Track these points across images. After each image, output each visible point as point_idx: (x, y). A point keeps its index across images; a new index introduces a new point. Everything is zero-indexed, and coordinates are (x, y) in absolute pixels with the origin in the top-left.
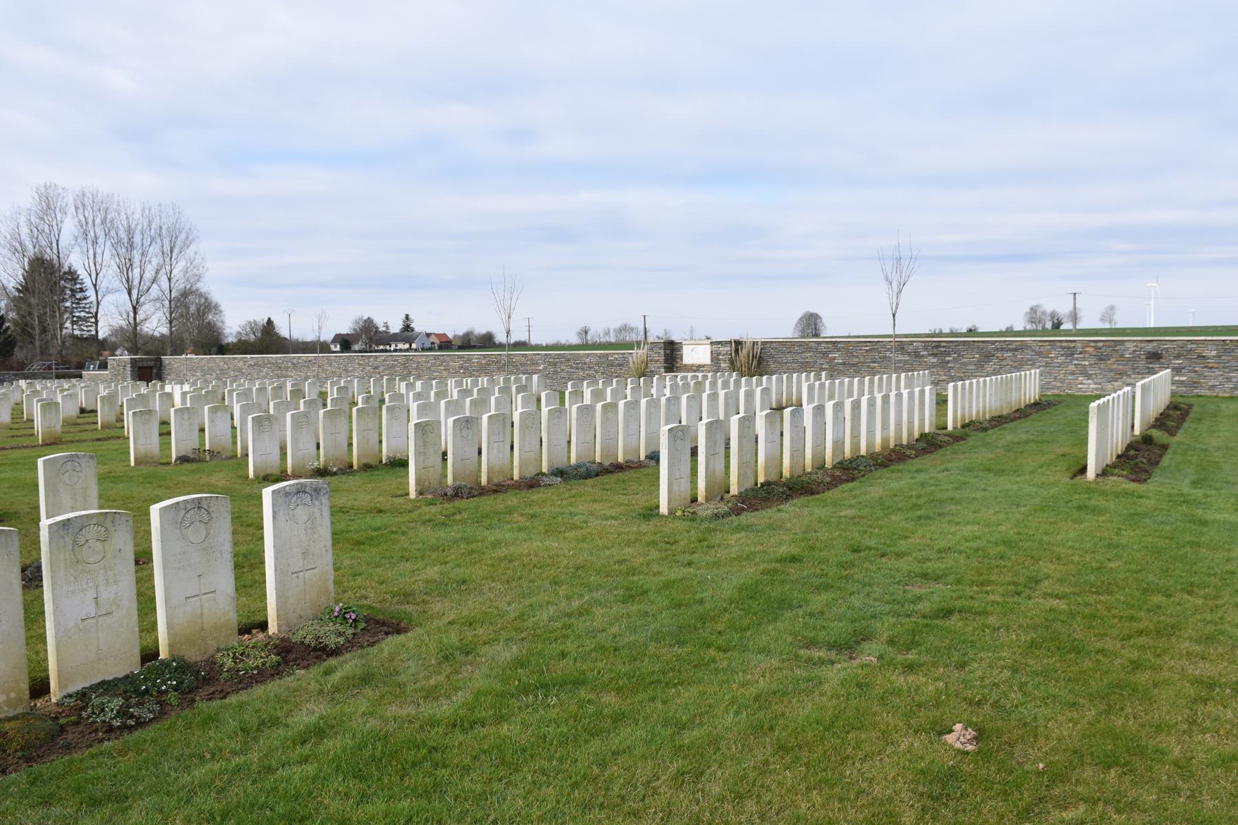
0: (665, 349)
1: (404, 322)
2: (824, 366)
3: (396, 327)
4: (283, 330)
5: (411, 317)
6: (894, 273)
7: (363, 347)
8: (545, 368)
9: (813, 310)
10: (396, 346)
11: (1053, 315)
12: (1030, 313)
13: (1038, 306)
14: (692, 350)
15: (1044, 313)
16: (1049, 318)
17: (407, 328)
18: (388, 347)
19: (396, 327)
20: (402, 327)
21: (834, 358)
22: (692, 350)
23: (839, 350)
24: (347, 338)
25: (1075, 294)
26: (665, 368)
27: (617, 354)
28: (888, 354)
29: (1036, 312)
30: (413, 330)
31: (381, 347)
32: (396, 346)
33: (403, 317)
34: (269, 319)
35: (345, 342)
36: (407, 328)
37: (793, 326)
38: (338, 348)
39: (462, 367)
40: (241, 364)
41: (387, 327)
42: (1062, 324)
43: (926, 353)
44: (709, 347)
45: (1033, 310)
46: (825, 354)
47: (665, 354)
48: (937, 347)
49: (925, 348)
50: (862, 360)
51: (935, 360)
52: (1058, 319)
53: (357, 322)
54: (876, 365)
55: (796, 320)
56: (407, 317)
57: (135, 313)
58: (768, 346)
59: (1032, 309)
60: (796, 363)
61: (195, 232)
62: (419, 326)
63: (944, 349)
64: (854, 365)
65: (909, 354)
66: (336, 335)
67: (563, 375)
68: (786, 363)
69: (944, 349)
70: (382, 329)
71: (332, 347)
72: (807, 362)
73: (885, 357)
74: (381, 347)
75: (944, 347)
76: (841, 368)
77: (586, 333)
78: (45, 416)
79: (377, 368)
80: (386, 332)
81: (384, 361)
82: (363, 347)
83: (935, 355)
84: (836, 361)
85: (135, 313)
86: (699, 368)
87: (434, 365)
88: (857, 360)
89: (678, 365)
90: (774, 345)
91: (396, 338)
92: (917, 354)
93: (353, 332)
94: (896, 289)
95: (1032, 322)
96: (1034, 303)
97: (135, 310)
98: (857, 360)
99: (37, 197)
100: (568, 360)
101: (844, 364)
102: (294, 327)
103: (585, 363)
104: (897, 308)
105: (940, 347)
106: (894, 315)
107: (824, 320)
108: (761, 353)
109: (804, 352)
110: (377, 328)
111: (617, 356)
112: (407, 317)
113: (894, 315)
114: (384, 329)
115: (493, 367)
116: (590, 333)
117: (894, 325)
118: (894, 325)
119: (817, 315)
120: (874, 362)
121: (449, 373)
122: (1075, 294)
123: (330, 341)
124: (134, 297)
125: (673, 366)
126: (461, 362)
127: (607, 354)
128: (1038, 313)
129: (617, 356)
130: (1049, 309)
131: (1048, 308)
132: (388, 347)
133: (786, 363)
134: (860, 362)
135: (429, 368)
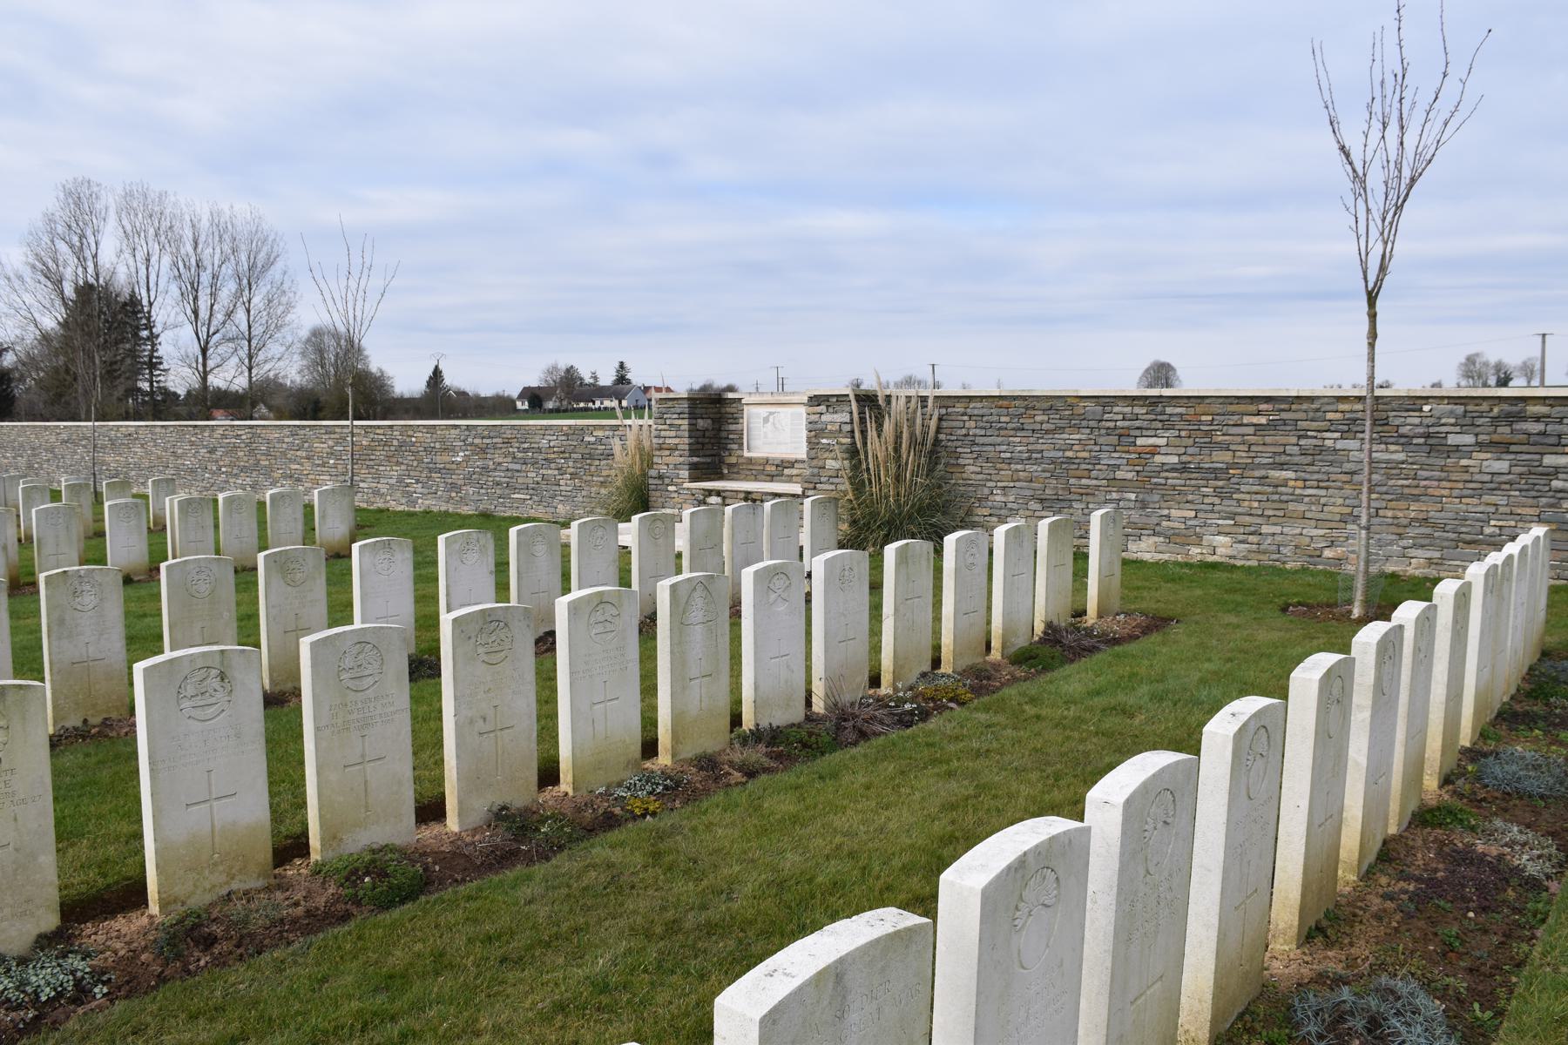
0: (693, 416)
1: (618, 371)
2: (1119, 474)
3: (607, 379)
4: (454, 379)
5: (627, 365)
6: (1375, 134)
7: (558, 404)
8: (467, 459)
9: (1163, 359)
10: (602, 403)
11: (1499, 367)
12: (1466, 365)
13: (1477, 355)
14: (766, 420)
15: (1486, 364)
16: (1493, 371)
17: (622, 379)
18: (590, 405)
19: (607, 379)
20: (615, 378)
21: (1154, 451)
22: (766, 420)
23: (1167, 425)
24: (537, 392)
25: (1544, 335)
26: (693, 467)
27: (602, 427)
28: (1330, 440)
29: (1474, 364)
30: (629, 382)
31: (582, 405)
32: (602, 403)
33: (617, 365)
34: (437, 367)
35: (535, 399)
36: (622, 379)
37: (1137, 380)
38: (526, 406)
39: (331, 454)
40: (53, 439)
41: (595, 378)
42: (1511, 379)
43: (1469, 439)
44: (803, 410)
45: (1471, 360)
46: (1124, 437)
47: (693, 429)
48: (1512, 418)
49: (1466, 423)
50: (1242, 457)
51: (1502, 466)
52: (1505, 373)
53: (550, 372)
54: (1291, 474)
55: (1141, 372)
56: (622, 365)
57: (205, 358)
58: (959, 409)
59: (1469, 359)
60: (1037, 462)
61: (281, 244)
62: (637, 377)
63: (1540, 427)
64: (1215, 473)
65: (1405, 441)
66: (525, 388)
67: (499, 476)
68: (1009, 461)
69: (1540, 427)
70: (588, 380)
71: (519, 405)
72: (1070, 460)
73: (1321, 450)
74: (582, 405)
75: (1538, 419)
76: (1174, 480)
77: (858, 386)
78: (157, 495)
79: (212, 451)
80: (594, 385)
81: (224, 436)
82: (558, 404)
83: (1501, 447)
84: (1158, 459)
85: (205, 358)
86: (779, 469)
87: (291, 445)
88: (1227, 457)
89: (733, 460)
90: (976, 408)
91: (603, 392)
92: (1433, 443)
93: (543, 385)
94: (1377, 203)
95: (1469, 377)
96: (1472, 351)
97: (204, 351)
98: (1227, 457)
99: (62, 195)
100: (508, 442)
101: (1183, 468)
102: (461, 378)
103: (539, 450)
104: (1383, 269)
105: (1524, 419)
106: (1372, 298)
107: (1179, 372)
108: (939, 430)
109: (1061, 429)
110: (581, 379)
111: (599, 433)
112: (622, 365)
113: (1372, 298)
114: (592, 381)
115: (380, 454)
116: (862, 387)
117: (1373, 335)
118: (1373, 335)
119: (1169, 365)
120: (1282, 466)
121: (314, 464)
122: (1544, 335)
123: (515, 395)
124: (203, 336)
125: (722, 462)
126: (331, 443)
127: (582, 429)
128: (1477, 365)
129: (599, 433)
130: (1493, 360)
131: (1492, 358)
132: (590, 405)
133: (1009, 461)
134: (1235, 465)
135: (284, 454)
